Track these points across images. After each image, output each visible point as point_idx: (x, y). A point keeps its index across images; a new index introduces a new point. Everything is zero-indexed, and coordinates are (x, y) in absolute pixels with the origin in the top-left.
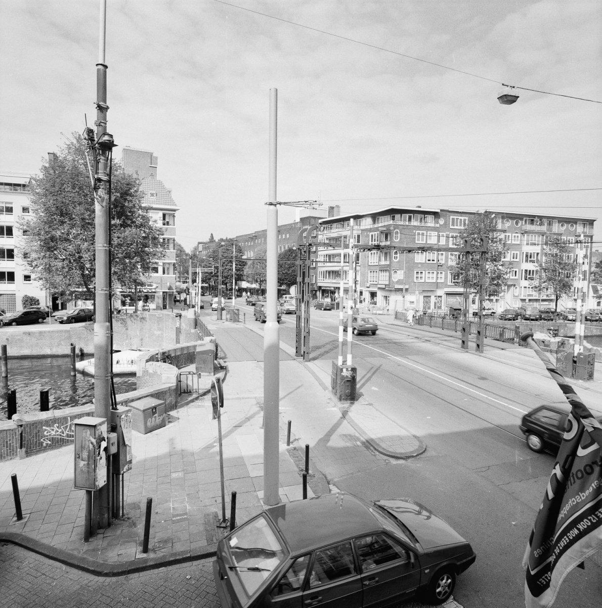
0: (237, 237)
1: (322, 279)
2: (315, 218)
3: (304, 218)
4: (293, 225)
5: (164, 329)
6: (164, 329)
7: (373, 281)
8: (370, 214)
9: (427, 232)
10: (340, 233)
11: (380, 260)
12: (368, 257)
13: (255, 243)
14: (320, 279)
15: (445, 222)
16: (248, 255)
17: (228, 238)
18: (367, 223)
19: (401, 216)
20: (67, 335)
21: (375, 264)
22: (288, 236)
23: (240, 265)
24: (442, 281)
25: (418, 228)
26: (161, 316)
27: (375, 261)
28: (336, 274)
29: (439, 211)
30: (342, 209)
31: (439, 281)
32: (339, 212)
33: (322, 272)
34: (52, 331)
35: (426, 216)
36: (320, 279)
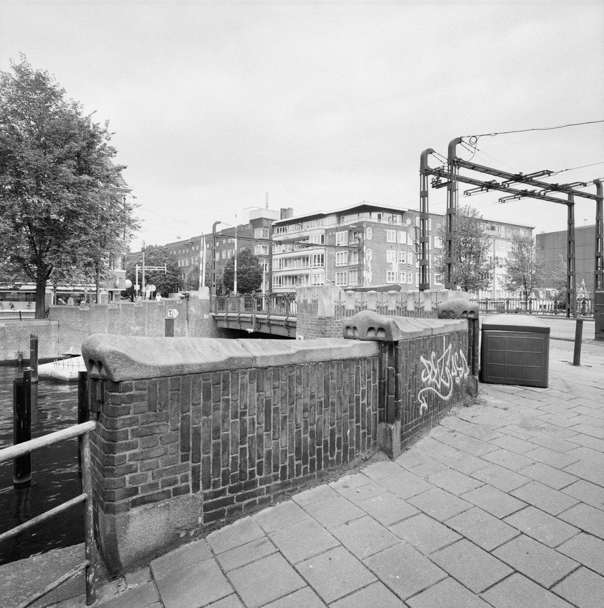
0: (167, 245)
1: (278, 285)
2: (268, 220)
3: (256, 220)
5: (146, 322)
6: (146, 322)
7: (342, 284)
8: (336, 213)
11: (349, 260)
12: (335, 258)
14: (276, 284)
16: (182, 263)
17: (158, 246)
18: (334, 219)
19: (370, 214)
21: (344, 265)
23: (174, 275)
24: (411, 283)
25: (389, 227)
26: (142, 306)
27: (344, 262)
28: (294, 278)
29: (407, 210)
31: (408, 283)
32: (292, 213)
33: (277, 277)
35: (394, 215)
36: (276, 284)
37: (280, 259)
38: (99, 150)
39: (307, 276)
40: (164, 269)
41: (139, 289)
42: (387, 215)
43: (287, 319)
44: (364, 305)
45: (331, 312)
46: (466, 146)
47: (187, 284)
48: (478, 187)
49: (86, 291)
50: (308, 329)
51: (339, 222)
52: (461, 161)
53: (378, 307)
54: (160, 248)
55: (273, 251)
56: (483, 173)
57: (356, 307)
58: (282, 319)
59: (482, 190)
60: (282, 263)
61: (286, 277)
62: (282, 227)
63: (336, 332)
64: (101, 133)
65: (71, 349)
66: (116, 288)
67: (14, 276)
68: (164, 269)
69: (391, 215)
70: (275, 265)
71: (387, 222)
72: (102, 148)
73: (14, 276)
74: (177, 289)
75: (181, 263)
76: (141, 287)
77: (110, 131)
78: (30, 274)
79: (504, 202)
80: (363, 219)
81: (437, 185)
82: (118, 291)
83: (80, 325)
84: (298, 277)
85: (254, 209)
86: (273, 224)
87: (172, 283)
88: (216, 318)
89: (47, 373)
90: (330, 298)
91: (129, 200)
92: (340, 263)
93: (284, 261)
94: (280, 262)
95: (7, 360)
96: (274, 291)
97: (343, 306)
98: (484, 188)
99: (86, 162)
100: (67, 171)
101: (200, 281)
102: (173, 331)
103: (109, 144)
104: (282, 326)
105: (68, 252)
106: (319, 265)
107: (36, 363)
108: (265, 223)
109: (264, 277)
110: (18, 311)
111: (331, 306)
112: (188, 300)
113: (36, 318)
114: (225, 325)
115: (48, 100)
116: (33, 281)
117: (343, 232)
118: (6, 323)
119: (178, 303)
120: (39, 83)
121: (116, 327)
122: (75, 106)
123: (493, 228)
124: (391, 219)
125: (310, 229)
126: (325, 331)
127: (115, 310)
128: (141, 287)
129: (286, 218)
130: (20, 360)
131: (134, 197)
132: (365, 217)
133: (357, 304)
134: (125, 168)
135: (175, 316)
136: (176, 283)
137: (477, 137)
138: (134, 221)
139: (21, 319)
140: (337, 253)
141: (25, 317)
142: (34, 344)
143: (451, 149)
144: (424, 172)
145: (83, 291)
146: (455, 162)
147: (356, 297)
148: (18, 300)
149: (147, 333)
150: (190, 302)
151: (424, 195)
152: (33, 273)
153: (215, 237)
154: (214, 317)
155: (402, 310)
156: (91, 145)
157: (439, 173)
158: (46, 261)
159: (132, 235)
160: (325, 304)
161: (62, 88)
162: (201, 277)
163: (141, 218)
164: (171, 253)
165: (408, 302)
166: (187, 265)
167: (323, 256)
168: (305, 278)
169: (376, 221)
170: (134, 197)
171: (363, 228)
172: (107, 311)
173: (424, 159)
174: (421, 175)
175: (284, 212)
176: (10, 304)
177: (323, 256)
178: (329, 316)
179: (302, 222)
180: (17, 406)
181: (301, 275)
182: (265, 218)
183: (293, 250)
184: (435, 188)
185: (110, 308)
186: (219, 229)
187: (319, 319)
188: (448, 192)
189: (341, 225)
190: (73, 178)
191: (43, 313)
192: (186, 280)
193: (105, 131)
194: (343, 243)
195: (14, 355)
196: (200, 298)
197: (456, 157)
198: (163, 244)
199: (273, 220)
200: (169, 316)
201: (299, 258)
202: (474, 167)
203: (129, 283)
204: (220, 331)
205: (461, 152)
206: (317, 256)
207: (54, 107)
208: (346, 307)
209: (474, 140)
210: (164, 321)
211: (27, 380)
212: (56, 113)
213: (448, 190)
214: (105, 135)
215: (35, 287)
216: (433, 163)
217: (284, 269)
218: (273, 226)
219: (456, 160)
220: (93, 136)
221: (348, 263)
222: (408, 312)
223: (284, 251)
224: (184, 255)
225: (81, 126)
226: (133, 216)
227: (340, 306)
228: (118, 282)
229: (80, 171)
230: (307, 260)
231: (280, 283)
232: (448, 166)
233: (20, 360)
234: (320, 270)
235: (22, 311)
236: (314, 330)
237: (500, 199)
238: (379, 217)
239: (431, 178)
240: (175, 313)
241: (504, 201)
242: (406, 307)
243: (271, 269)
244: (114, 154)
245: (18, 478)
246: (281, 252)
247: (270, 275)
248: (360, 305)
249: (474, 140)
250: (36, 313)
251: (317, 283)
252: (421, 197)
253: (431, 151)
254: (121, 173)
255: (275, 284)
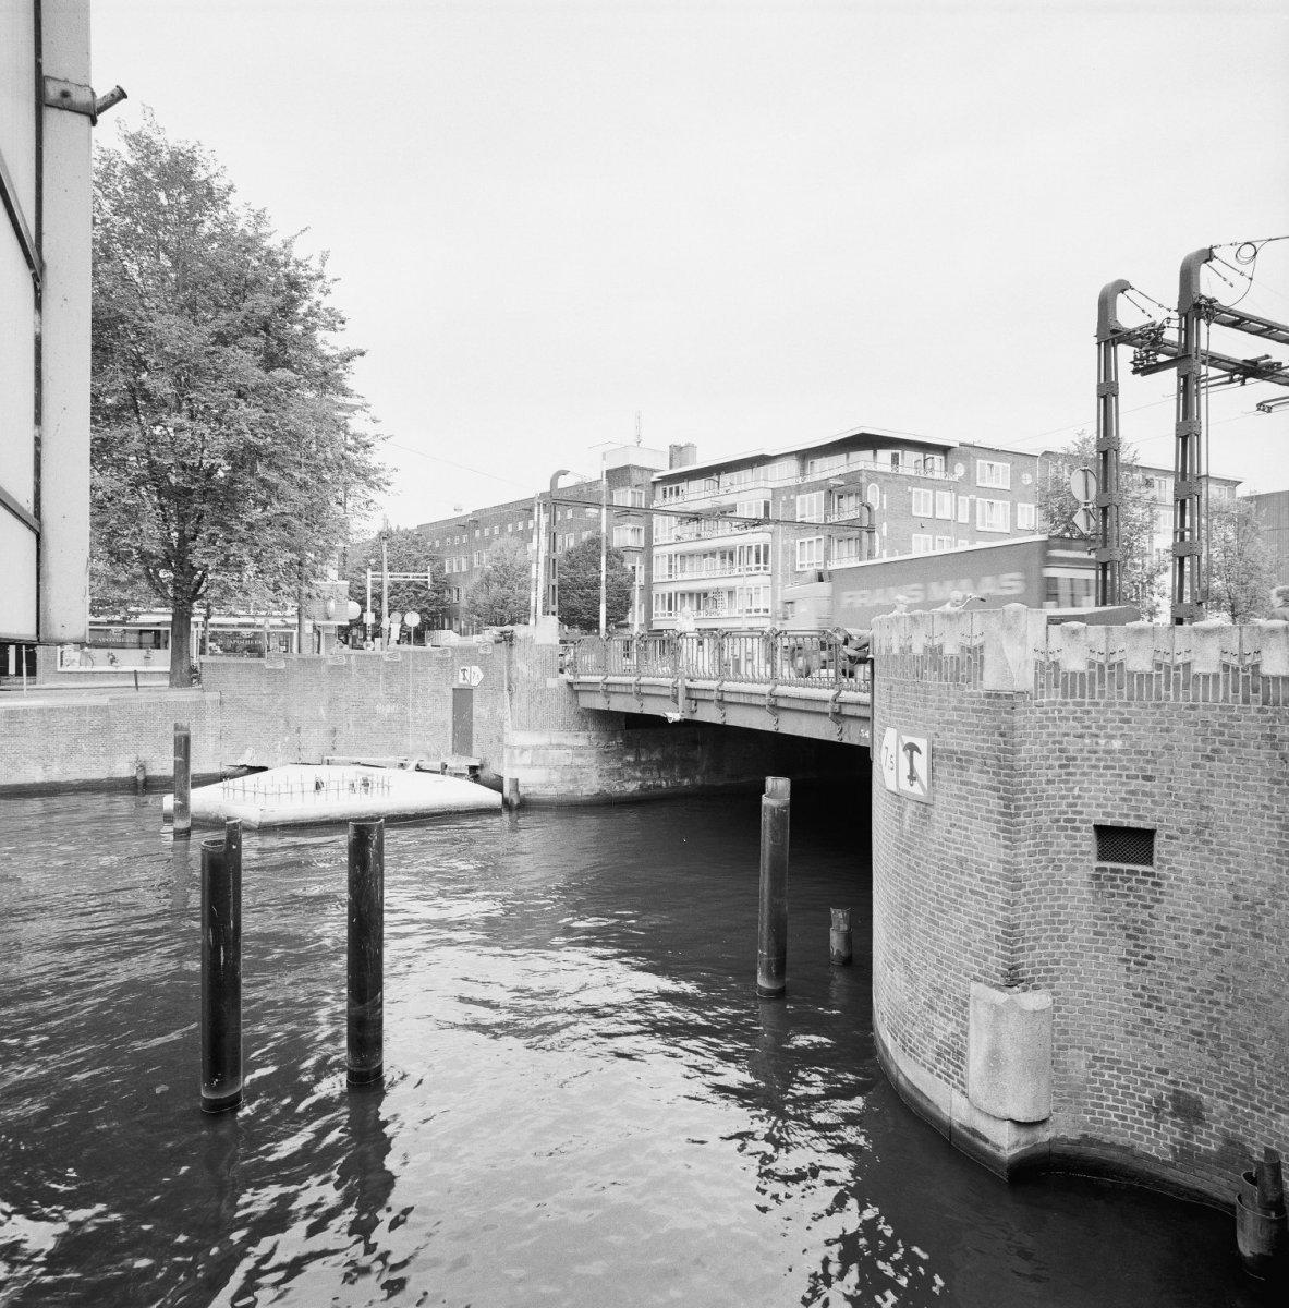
0: (420, 527)
2: (642, 469)
3: (616, 470)
4: (585, 489)
5: (410, 696)
8: (796, 453)
9: (934, 492)
10: (717, 499)
11: (827, 557)
12: (794, 552)
13: (471, 537)
15: (968, 472)
16: (453, 565)
17: (401, 529)
18: (792, 466)
19: (875, 454)
20: (97, 720)
22: (570, 516)
30: (699, 452)
32: (695, 454)
34: (51, 710)
35: (928, 456)
36: (660, 611)
37: (670, 556)
38: (306, 315)
39: (731, 593)
40: (426, 577)
41: (374, 622)
42: (910, 458)
43: (773, 690)
44: (1115, 659)
45: (1025, 680)
46: (1226, 271)
47: (467, 611)
48: (1223, 372)
49: (267, 626)
50: (948, 722)
51: (803, 472)
52: (1214, 304)
53: (1159, 666)
54: (407, 534)
55: (654, 537)
56: (1254, 336)
57: (1091, 664)
58: (823, 698)
59: (1232, 381)
60: (674, 564)
61: (683, 595)
62: (674, 486)
63: (1037, 730)
64: (311, 278)
65: (248, 753)
66: (328, 619)
67: (129, 592)
68: (426, 577)
69: (920, 456)
70: (660, 570)
71: (912, 472)
72: (311, 313)
73: (129, 592)
74: (443, 623)
75: (451, 567)
76: (379, 617)
77: (329, 273)
78: (158, 587)
79: (1269, 411)
80: (861, 466)
81: (1144, 368)
82: (328, 627)
83: (265, 700)
84: (710, 595)
85: (615, 447)
86: (653, 479)
87: (433, 609)
88: (576, 687)
89: (208, 810)
90: (1023, 642)
91: (357, 424)
92: (806, 562)
93: (678, 558)
94: (671, 561)
95: (112, 779)
96: (656, 626)
97: (1056, 663)
98: (1236, 376)
99: (281, 341)
100: (243, 361)
101: (533, 604)
102: (471, 715)
103: (327, 302)
104: (630, 694)
105: (242, 540)
106: (758, 568)
107: (186, 788)
108: (636, 477)
109: (637, 596)
110: (132, 669)
111: (1026, 661)
112: (511, 645)
113: (171, 685)
114: (599, 703)
115: (193, 207)
116: (166, 606)
117: (814, 495)
118: (111, 696)
119: (482, 651)
120: (178, 172)
121: (344, 706)
122: (260, 217)
123: (1148, 483)
124: (921, 464)
125: (737, 488)
126: (1013, 728)
127: (339, 668)
128: (379, 617)
129: (680, 466)
130: (141, 778)
131: (374, 421)
132: (862, 460)
133: (1094, 657)
134: (362, 354)
135: (475, 683)
136: (441, 608)
137: (1257, 245)
138: (376, 471)
139: (137, 687)
140: (798, 541)
141: (145, 684)
142: (183, 746)
143: (1188, 276)
144: (1110, 336)
145: (259, 626)
146: (1196, 309)
147: (1092, 638)
148: (122, 646)
149: (411, 720)
150: (515, 650)
151: (1107, 393)
152: (165, 587)
153: (554, 501)
154: (570, 684)
155: (1241, 674)
156: (287, 309)
157: (1150, 338)
158: (197, 559)
159: (372, 501)
160: (1009, 656)
161: (229, 184)
162: (533, 594)
163: (388, 466)
164: (429, 544)
165: (1264, 652)
166: (464, 569)
167: (766, 548)
168: (726, 596)
169: (888, 469)
170: (374, 421)
171: (860, 484)
172: (323, 668)
173: (1106, 304)
174: (1099, 344)
175: (677, 451)
176: (109, 654)
177: (766, 548)
178: (1021, 689)
179: (719, 474)
180: (212, 912)
181: (718, 591)
182: (635, 467)
183: (699, 535)
184: (1139, 375)
185: (330, 663)
186: (563, 483)
187: (989, 696)
188: (1099, 401)
189: (808, 479)
190: (256, 375)
191: (185, 675)
192: (464, 603)
193: (320, 277)
194: (816, 517)
195: (127, 766)
196: (538, 641)
197: (1201, 297)
198: (412, 526)
199: (652, 471)
200: (460, 681)
201: (713, 554)
202: (1239, 322)
203: (354, 609)
204: (583, 716)
205: (1209, 284)
206: (754, 549)
207: (208, 223)
208: (1062, 665)
209: (1249, 251)
210: (451, 692)
211: (234, 847)
212: (212, 238)
213: (1179, 376)
214: (319, 283)
215: (169, 618)
216: (1129, 316)
217: (679, 577)
218: (654, 483)
219: (1203, 301)
220: (293, 284)
221: (825, 564)
222: (1266, 678)
223: (679, 538)
224: (457, 549)
225: (270, 259)
226: (373, 460)
227: (1047, 663)
228: (332, 605)
229: (270, 362)
230: (732, 558)
231: (670, 608)
232: (1180, 319)
233: (141, 778)
234: (762, 579)
235: (139, 669)
236: (971, 724)
237: (1260, 404)
238: (895, 459)
239: (1125, 354)
240: (474, 676)
241: (1270, 408)
242: (1256, 667)
243: (649, 577)
244: (338, 326)
245: (211, 1089)
246: (674, 540)
247: (648, 587)
248: (1102, 659)
249: (1249, 251)
250: (171, 675)
251: (754, 608)
252: (1099, 396)
253: (1122, 287)
254: (351, 363)
255: (659, 610)
